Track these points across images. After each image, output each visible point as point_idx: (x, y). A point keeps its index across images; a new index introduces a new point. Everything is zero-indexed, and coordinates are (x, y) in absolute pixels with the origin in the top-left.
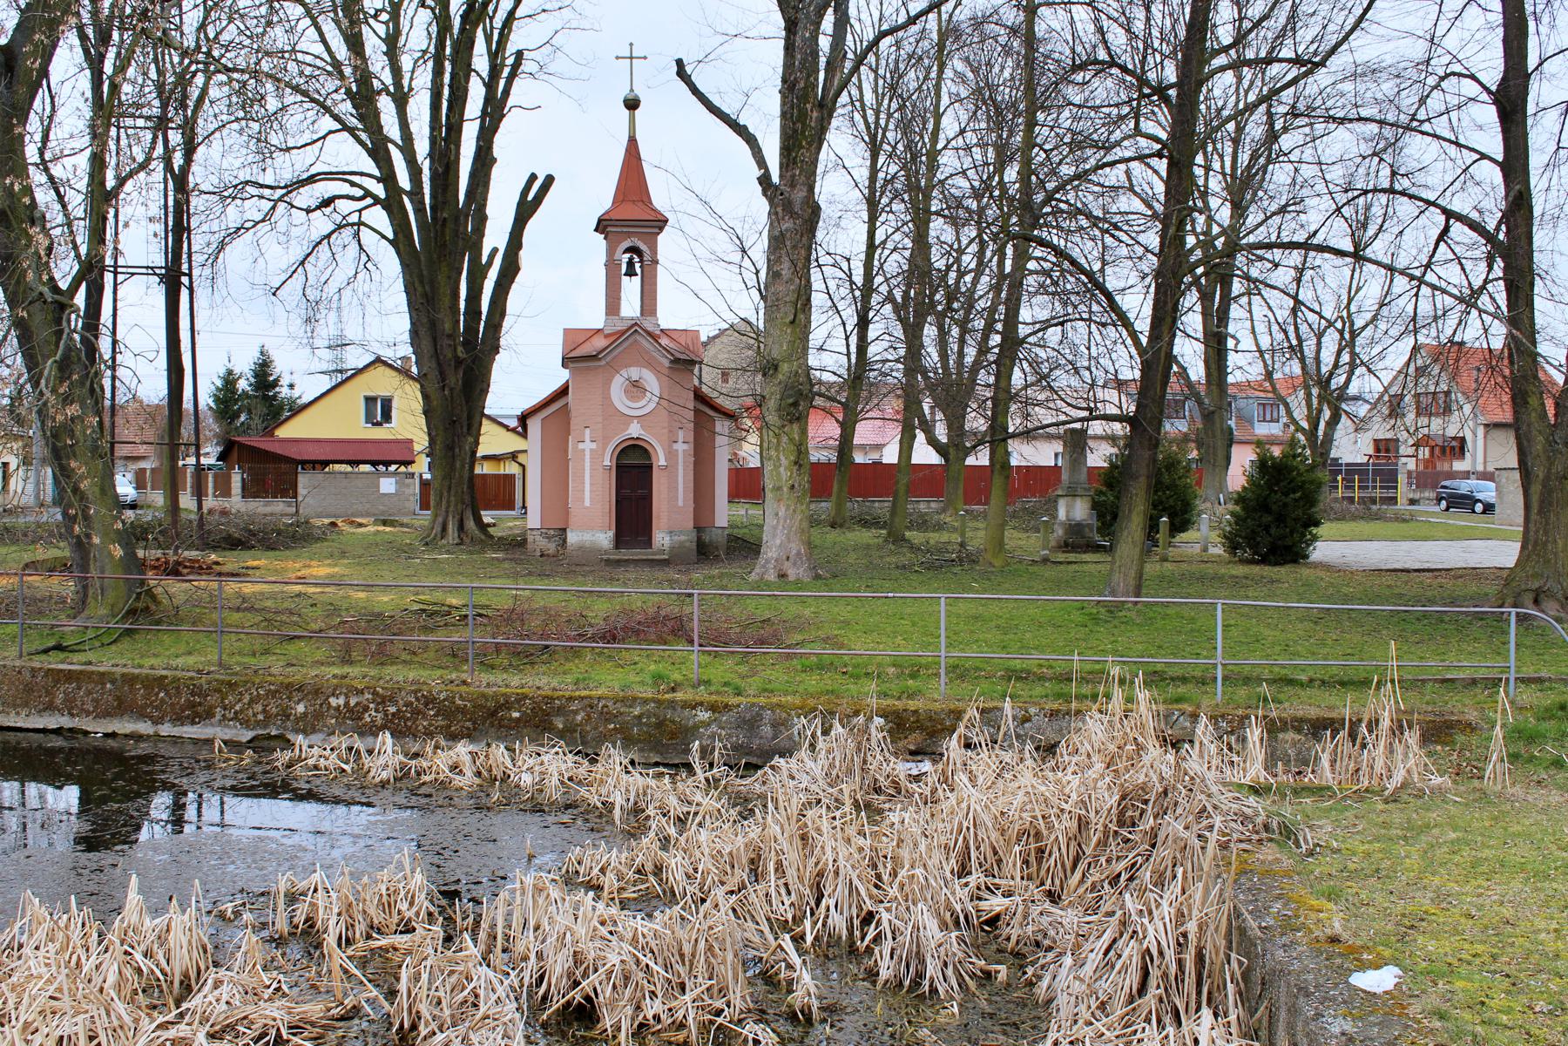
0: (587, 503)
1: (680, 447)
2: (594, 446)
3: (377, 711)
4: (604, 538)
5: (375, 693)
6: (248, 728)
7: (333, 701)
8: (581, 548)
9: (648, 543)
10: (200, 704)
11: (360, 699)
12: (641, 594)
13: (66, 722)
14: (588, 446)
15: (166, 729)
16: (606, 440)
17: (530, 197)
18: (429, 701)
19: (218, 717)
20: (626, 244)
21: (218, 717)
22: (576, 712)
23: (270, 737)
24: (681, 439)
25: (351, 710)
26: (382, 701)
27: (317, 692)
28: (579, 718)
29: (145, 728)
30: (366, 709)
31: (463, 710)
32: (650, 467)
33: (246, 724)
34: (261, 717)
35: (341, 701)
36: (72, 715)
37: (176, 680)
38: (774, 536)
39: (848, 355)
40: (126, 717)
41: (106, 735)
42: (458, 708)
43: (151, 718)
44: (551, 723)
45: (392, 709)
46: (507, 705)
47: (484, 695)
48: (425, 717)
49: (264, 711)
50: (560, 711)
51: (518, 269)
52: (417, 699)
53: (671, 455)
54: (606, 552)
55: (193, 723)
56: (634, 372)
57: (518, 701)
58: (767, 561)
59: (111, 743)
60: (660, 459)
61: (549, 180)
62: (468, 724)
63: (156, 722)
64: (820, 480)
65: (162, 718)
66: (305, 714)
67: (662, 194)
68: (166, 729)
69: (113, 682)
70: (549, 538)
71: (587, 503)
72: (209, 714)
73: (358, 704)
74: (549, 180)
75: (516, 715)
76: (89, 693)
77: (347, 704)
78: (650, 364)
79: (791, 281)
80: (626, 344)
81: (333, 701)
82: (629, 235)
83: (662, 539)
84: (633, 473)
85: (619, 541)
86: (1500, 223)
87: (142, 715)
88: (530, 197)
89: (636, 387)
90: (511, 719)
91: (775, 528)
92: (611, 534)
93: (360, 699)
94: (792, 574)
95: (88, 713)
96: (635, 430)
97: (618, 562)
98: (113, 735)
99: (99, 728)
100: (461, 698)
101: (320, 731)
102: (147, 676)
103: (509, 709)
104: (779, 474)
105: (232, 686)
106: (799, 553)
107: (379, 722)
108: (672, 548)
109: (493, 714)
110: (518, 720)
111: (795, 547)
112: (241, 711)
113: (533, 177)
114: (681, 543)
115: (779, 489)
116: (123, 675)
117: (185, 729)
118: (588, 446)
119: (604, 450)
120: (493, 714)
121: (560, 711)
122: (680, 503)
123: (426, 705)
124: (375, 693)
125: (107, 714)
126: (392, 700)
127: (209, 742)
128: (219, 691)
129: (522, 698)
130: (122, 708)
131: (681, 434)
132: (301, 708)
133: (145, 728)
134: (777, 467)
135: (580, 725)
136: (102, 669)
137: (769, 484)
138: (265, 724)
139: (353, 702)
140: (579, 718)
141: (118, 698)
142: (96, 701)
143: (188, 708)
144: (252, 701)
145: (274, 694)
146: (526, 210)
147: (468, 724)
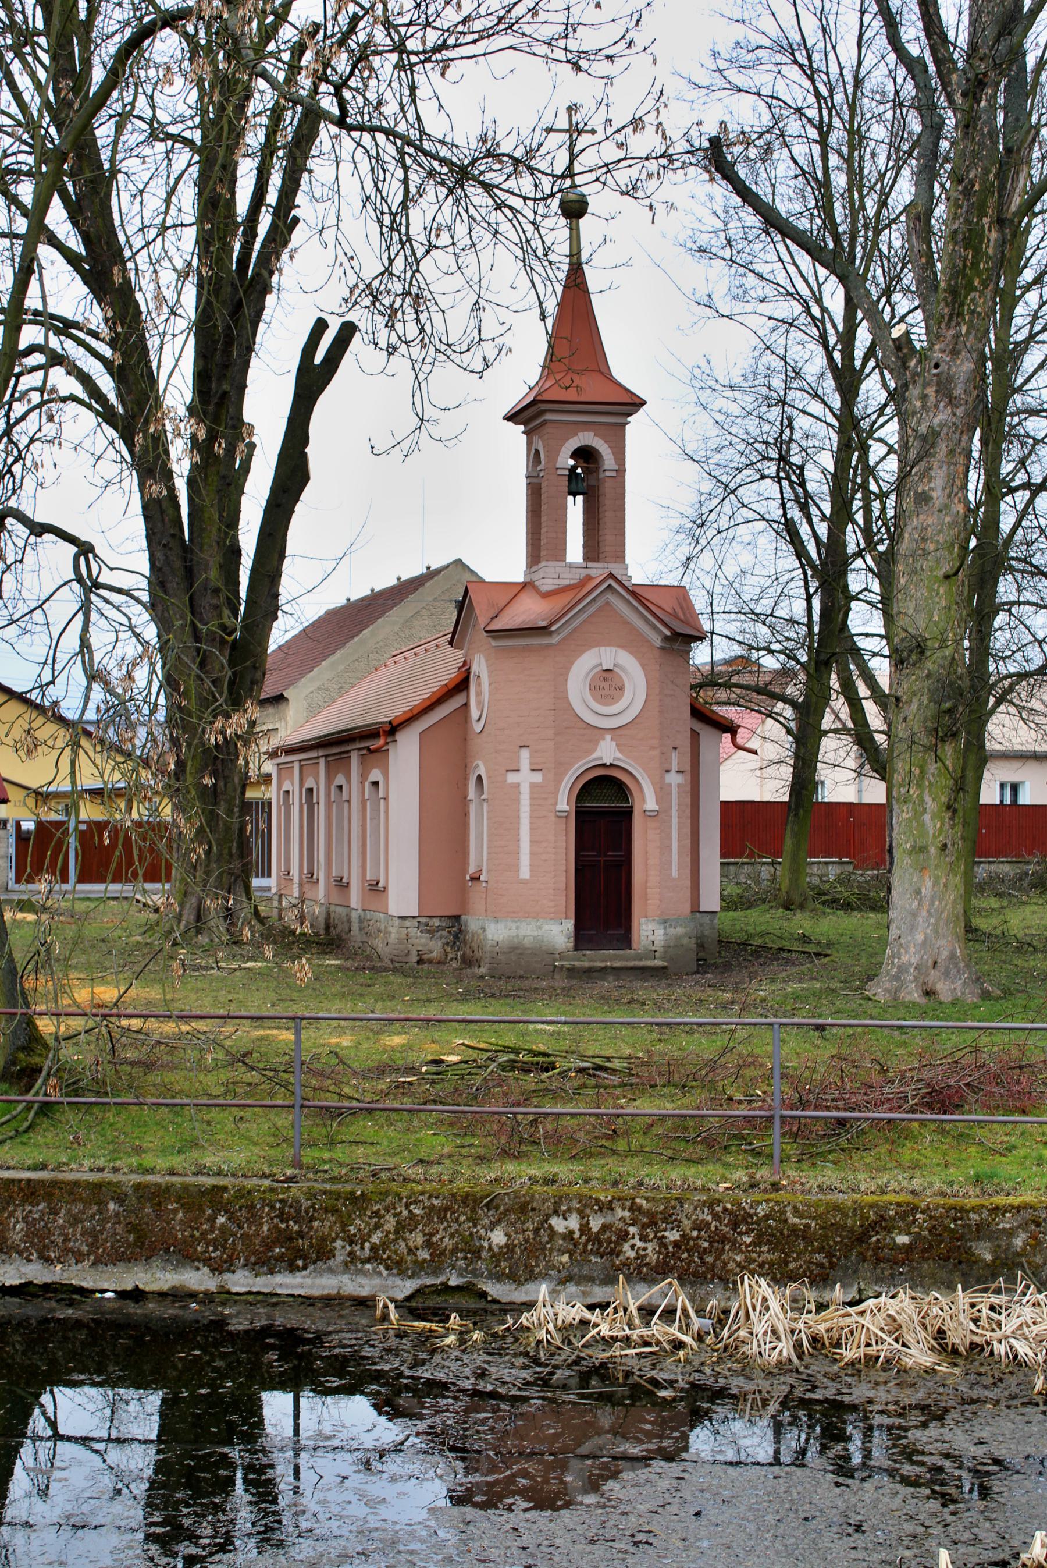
0: (525, 873)
2: (538, 777)
3: (643, 1238)
4: (558, 932)
5: (634, 1208)
6: (402, 1273)
7: (558, 1224)
8: (516, 949)
9: (625, 940)
10: (301, 1234)
11: (609, 1219)
12: (610, 1031)
13: (36, 1272)
14: (525, 778)
15: (240, 1281)
16: (560, 768)
17: (318, 359)
18: (739, 1219)
19: (340, 1257)
20: (573, 444)
21: (340, 1257)
22: (1011, 1233)
23: (446, 1289)
24: (675, 767)
25: (595, 1239)
26: (650, 1222)
27: (524, 1208)
28: (1018, 1242)
29: (198, 1279)
30: (624, 1236)
31: (805, 1234)
32: (628, 813)
33: (398, 1267)
34: (424, 1255)
35: (573, 1223)
36: (48, 1260)
37: (243, 1193)
38: (913, 928)
39: (810, 625)
40: (156, 1262)
41: (122, 1295)
42: (794, 1229)
43: (207, 1261)
44: (969, 1251)
45: (673, 1236)
46: (883, 1223)
47: (837, 1208)
48: (736, 1247)
49: (428, 1244)
50: (981, 1231)
51: (305, 478)
52: (716, 1216)
53: (662, 792)
54: (562, 956)
55: (293, 1268)
56: (608, 656)
57: (903, 1216)
58: (902, 969)
59: (132, 1309)
60: (646, 799)
61: (348, 331)
62: (819, 1257)
63: (217, 1269)
64: (744, 824)
65: (230, 1260)
66: (509, 1248)
67: (627, 361)
68: (240, 1281)
69: (121, 1200)
70: (431, 932)
71: (525, 873)
72: (322, 1253)
73: (605, 1228)
74: (348, 331)
75: (903, 1239)
76: (75, 1220)
77: (585, 1228)
78: (633, 643)
79: (944, 509)
80: (592, 609)
81: (558, 1224)
82: (586, 426)
83: (651, 931)
84: (603, 817)
85: (583, 937)
86: (868, 375)
87: (187, 1257)
88: (318, 359)
89: (607, 684)
90: (895, 1247)
91: (914, 915)
92: (570, 924)
93: (609, 1219)
94: (945, 989)
95: (80, 1257)
96: (607, 752)
97: (590, 973)
98: (137, 1295)
99: (108, 1281)
100: (796, 1211)
101: (544, 1277)
102: (186, 1187)
103: (889, 1230)
104: (922, 825)
105: (358, 1202)
106: (952, 956)
107: (652, 1258)
108: (666, 947)
109: (862, 1238)
110: (908, 1249)
111: (948, 945)
112: (384, 1245)
113: (320, 326)
114: (678, 938)
115: (923, 849)
116: (138, 1187)
117: (279, 1279)
118: (525, 778)
119: (558, 782)
120: (862, 1238)
121: (981, 1231)
122: (675, 874)
123: (735, 1226)
124: (634, 1208)
125: (119, 1257)
126: (669, 1218)
127: (365, 1303)
128: (335, 1211)
129: (907, 1211)
130: (142, 1246)
131: (674, 757)
132: (498, 1237)
133: (198, 1279)
134: (918, 814)
135: (1023, 1253)
136: (70, 1177)
137: (901, 838)
138: (435, 1265)
139: (596, 1224)
140: (1018, 1242)
141: (133, 1228)
142: (93, 1235)
143: (277, 1242)
144: (401, 1228)
145: (442, 1213)
146: (312, 380)
147: (819, 1257)
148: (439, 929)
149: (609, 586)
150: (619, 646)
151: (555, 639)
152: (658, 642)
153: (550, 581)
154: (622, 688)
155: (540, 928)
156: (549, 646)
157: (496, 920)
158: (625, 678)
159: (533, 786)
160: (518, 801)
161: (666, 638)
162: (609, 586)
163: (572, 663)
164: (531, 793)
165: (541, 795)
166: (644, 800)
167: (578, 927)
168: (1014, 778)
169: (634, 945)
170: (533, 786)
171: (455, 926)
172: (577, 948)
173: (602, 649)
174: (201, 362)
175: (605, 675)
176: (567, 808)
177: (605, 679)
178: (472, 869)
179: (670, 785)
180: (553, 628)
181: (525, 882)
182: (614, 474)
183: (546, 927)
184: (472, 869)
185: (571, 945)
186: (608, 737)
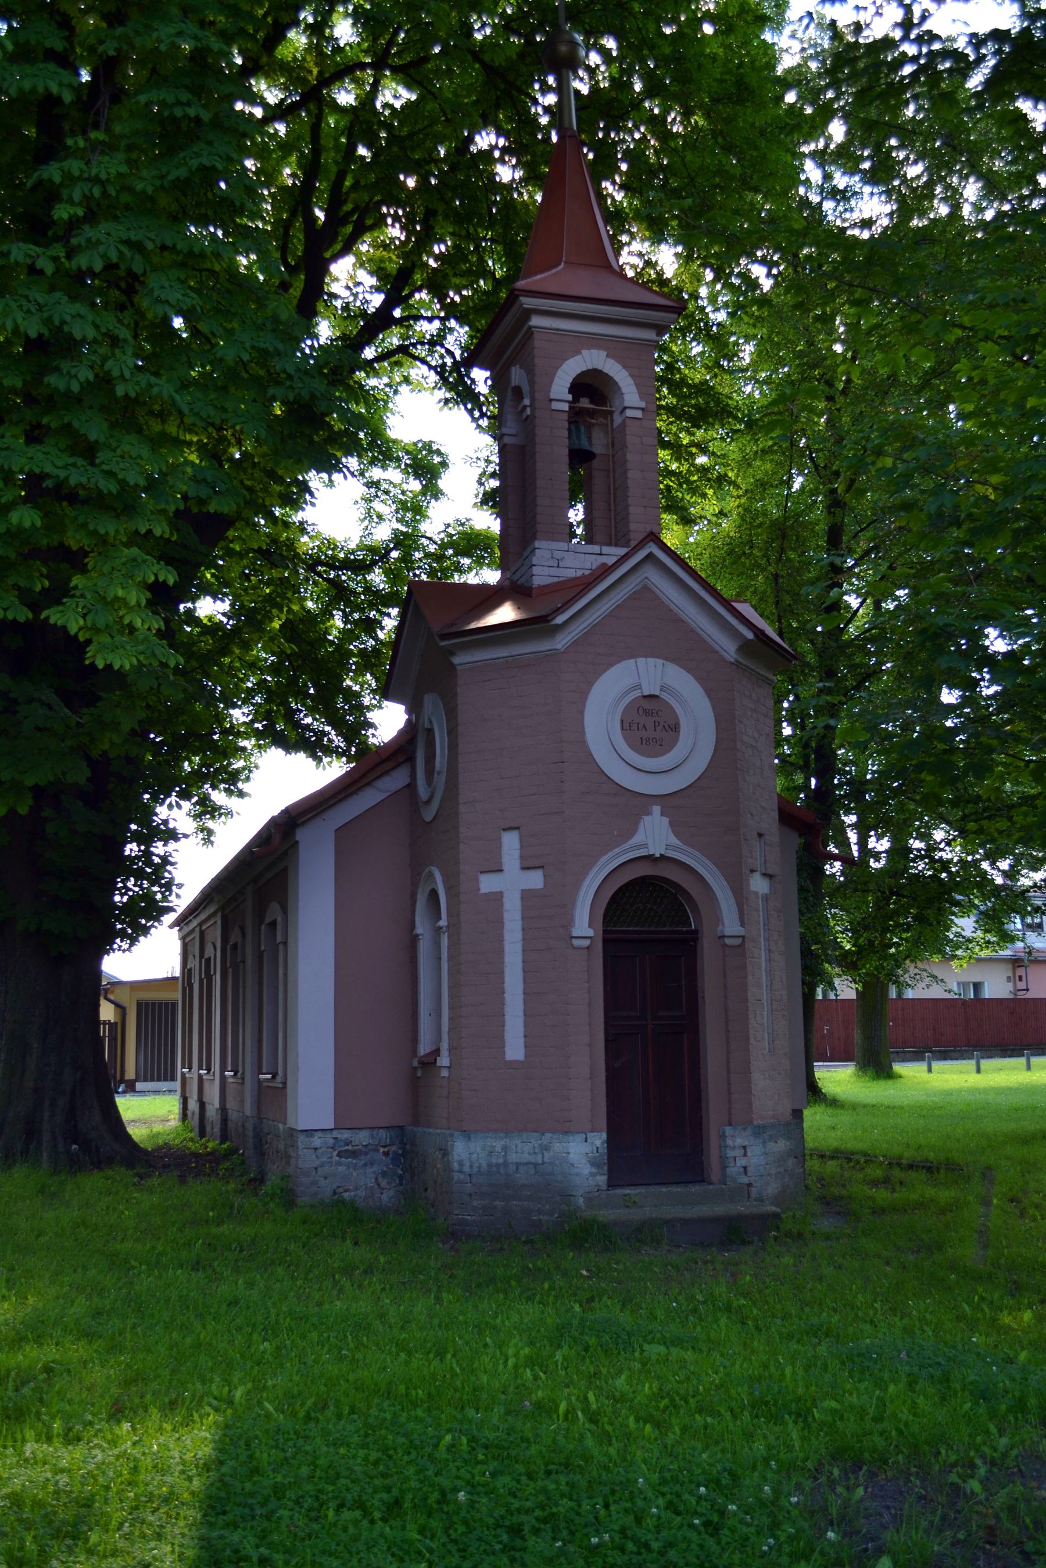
0: (515, 1049)
1: (758, 885)
4: (580, 1154)
71: (515, 1049)
78: (689, 652)
85: (622, 1162)
89: (650, 724)
96: (655, 835)
97: (644, 1234)
148: (368, 1149)
149: (650, 556)
150: (667, 659)
151: (561, 642)
152: (729, 648)
153: (547, 571)
154: (675, 728)
155: (546, 1148)
156: (553, 655)
157: (467, 1134)
158: (679, 711)
159: (526, 895)
160: (500, 923)
161: (745, 647)
162: (650, 556)
163: (591, 684)
164: (525, 908)
165: (545, 912)
166: (718, 919)
167: (612, 1143)
168: (977, 980)
169: (715, 1175)
170: (526, 895)
171: (408, 1155)
172: (611, 1184)
173: (641, 661)
174: (259, 846)
175: (647, 705)
176: (590, 933)
177: (647, 712)
178: (423, 1049)
179: (497, 898)
180: (560, 620)
181: (513, 1065)
182: (638, 414)
183: (557, 1147)
184: (423, 1049)
185: (602, 1179)
186: (657, 809)
